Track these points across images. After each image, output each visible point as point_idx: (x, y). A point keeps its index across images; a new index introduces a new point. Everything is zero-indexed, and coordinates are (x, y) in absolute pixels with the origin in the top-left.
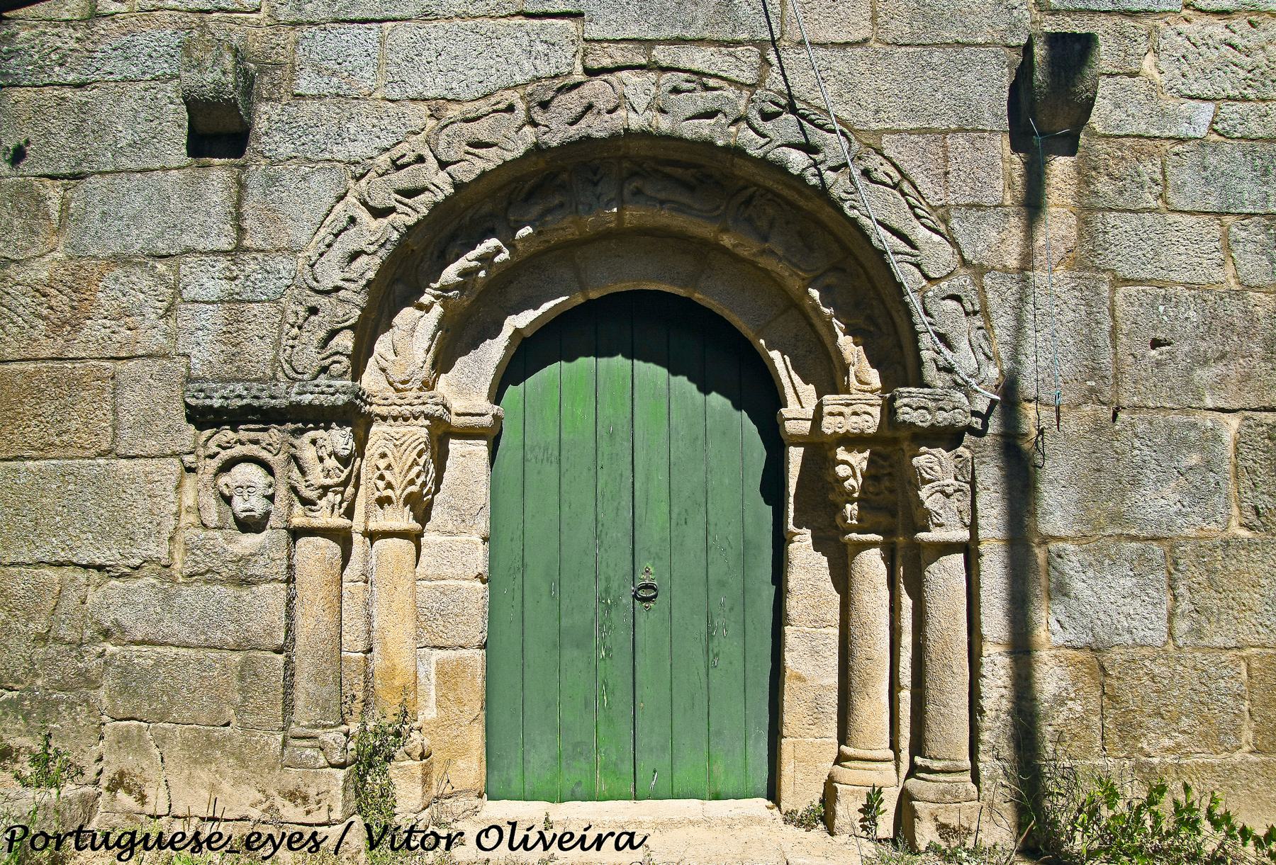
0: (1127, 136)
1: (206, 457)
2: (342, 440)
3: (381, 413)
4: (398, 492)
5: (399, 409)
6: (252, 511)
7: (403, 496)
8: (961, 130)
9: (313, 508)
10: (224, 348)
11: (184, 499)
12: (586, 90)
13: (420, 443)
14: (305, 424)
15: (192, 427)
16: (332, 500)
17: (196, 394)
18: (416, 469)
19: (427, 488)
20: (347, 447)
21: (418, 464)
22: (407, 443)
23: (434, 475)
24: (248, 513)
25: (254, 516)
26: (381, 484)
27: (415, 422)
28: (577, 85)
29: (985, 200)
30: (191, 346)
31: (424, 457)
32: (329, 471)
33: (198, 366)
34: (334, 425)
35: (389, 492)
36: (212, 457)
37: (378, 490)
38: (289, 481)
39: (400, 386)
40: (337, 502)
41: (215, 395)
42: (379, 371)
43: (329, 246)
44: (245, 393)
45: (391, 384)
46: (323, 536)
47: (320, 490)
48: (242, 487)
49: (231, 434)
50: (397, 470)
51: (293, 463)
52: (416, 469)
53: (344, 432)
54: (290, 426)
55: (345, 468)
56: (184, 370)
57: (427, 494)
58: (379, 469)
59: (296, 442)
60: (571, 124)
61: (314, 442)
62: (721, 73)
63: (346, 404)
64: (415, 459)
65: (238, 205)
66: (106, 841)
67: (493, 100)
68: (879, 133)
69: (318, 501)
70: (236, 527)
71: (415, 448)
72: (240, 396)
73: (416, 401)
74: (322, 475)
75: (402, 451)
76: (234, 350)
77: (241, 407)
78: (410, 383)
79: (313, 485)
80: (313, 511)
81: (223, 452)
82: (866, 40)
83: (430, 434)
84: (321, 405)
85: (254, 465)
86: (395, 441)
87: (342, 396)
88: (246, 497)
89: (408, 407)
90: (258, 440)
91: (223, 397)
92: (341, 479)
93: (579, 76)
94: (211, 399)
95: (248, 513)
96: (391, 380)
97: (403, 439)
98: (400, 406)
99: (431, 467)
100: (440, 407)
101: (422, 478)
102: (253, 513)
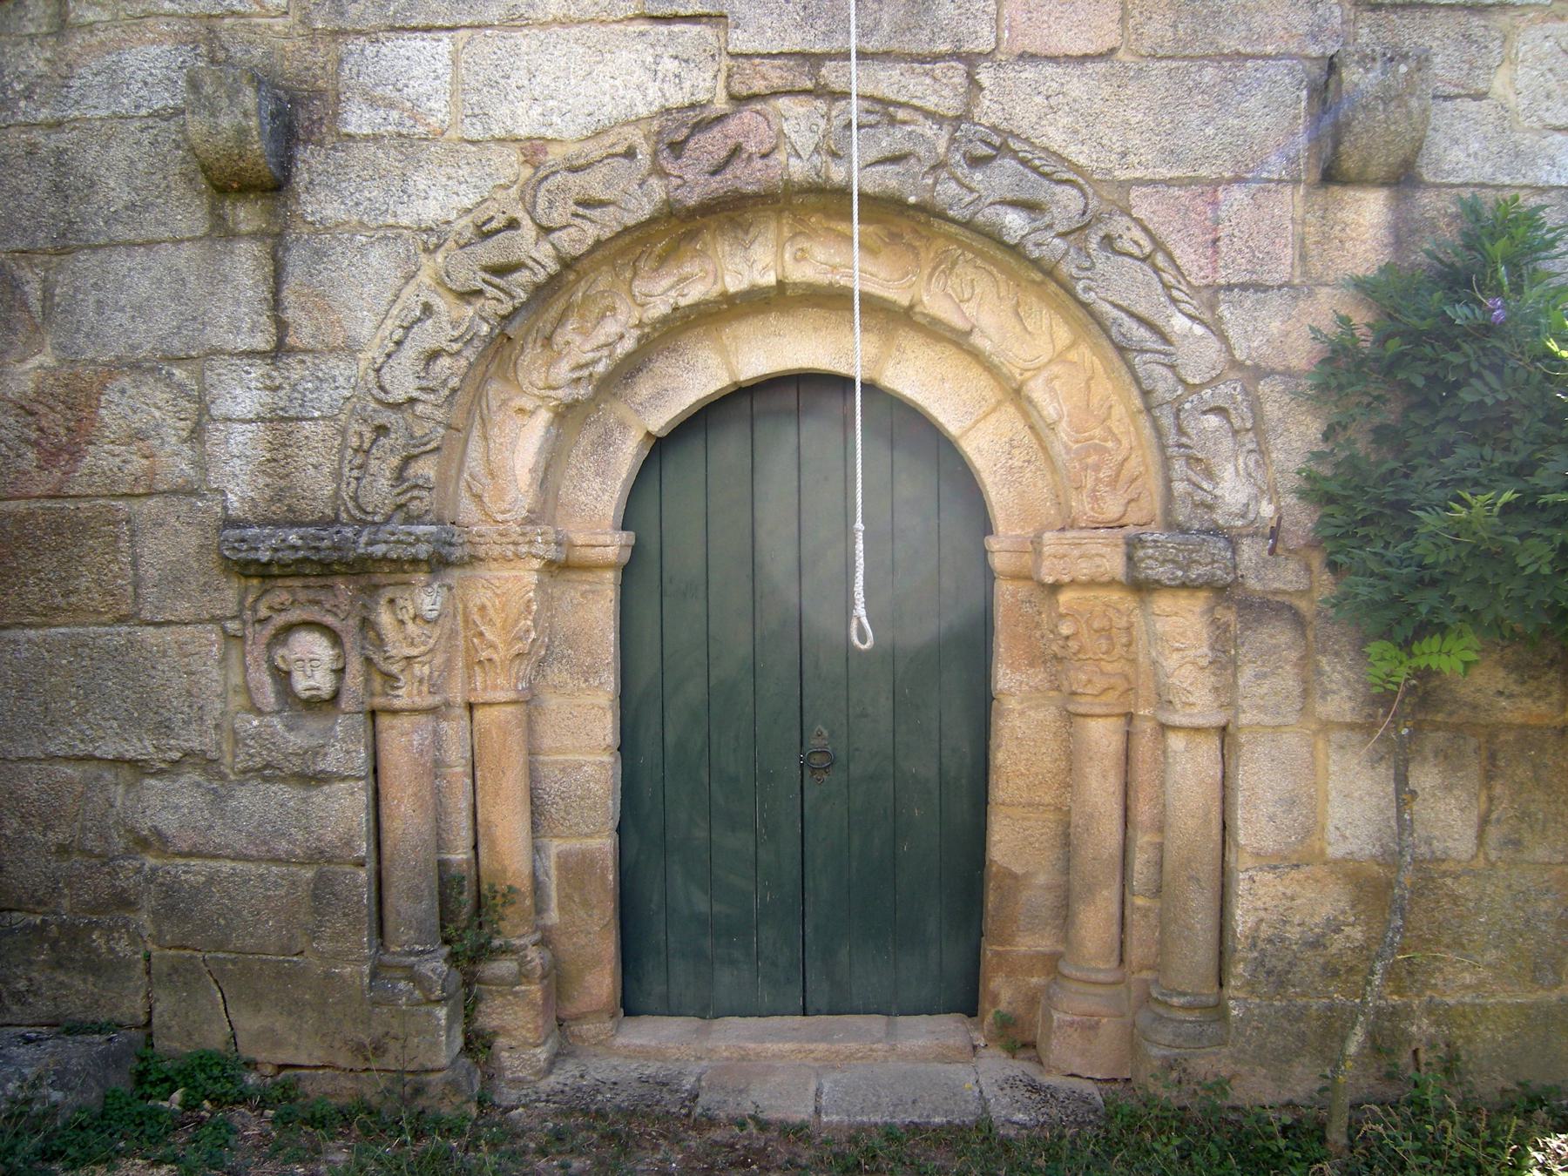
0: (1466, 185)
6: (318, 689)
8: (1238, 180)
10: (269, 480)
12: (732, 126)
28: (721, 119)
29: (1266, 276)
43: (399, 343)
60: (714, 173)
62: (915, 102)
65: (276, 292)
67: (612, 139)
68: (1126, 185)
82: (1112, 51)
89: (510, 547)
93: (721, 104)
95: (314, 692)
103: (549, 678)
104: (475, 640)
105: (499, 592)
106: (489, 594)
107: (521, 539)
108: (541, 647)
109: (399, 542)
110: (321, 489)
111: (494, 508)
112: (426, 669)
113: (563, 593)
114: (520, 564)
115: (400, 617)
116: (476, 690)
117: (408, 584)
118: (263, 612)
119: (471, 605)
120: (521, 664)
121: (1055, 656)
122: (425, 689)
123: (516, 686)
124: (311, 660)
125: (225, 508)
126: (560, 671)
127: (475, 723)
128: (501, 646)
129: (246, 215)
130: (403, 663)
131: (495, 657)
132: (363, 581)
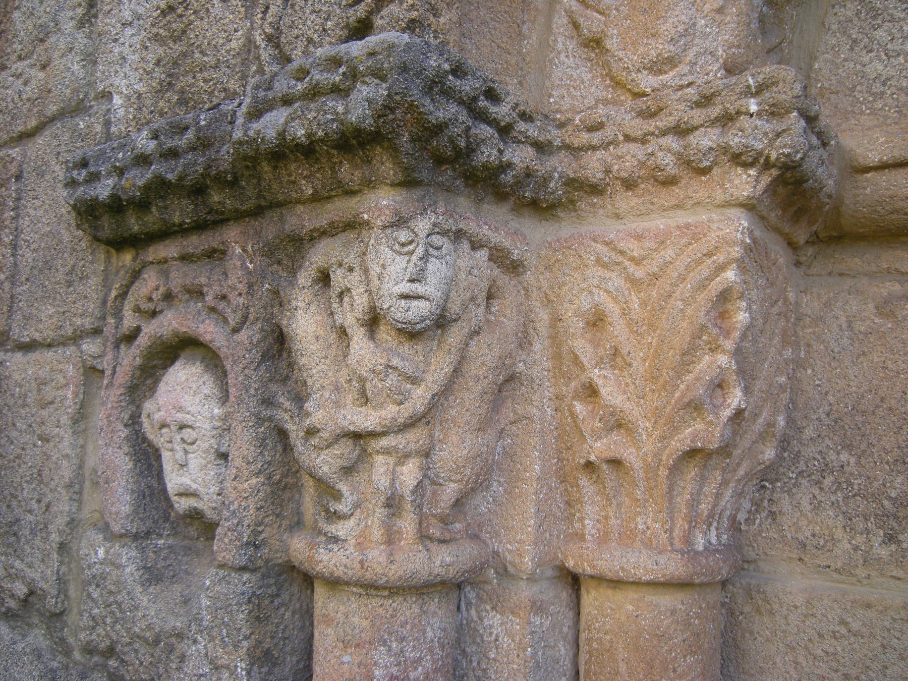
6: (194, 494)
20: (419, 288)
42: (583, 52)
71: (702, 286)
76: (179, 48)
86: (632, 268)
89: (671, 141)
103: (786, 521)
104: (579, 407)
105: (639, 273)
106: (616, 281)
107: (697, 116)
108: (762, 437)
111: (631, 58)
112: (409, 474)
113: (827, 305)
114: (696, 189)
115: (339, 320)
116: (582, 537)
117: (353, 225)
118: (129, 320)
119: (568, 312)
120: (702, 479)
121: (69, 523)
122: (407, 524)
123: (688, 540)
124: (182, 427)
126: (817, 507)
127: (583, 618)
128: (644, 425)
130: (345, 449)
131: (630, 455)
132: (269, 228)
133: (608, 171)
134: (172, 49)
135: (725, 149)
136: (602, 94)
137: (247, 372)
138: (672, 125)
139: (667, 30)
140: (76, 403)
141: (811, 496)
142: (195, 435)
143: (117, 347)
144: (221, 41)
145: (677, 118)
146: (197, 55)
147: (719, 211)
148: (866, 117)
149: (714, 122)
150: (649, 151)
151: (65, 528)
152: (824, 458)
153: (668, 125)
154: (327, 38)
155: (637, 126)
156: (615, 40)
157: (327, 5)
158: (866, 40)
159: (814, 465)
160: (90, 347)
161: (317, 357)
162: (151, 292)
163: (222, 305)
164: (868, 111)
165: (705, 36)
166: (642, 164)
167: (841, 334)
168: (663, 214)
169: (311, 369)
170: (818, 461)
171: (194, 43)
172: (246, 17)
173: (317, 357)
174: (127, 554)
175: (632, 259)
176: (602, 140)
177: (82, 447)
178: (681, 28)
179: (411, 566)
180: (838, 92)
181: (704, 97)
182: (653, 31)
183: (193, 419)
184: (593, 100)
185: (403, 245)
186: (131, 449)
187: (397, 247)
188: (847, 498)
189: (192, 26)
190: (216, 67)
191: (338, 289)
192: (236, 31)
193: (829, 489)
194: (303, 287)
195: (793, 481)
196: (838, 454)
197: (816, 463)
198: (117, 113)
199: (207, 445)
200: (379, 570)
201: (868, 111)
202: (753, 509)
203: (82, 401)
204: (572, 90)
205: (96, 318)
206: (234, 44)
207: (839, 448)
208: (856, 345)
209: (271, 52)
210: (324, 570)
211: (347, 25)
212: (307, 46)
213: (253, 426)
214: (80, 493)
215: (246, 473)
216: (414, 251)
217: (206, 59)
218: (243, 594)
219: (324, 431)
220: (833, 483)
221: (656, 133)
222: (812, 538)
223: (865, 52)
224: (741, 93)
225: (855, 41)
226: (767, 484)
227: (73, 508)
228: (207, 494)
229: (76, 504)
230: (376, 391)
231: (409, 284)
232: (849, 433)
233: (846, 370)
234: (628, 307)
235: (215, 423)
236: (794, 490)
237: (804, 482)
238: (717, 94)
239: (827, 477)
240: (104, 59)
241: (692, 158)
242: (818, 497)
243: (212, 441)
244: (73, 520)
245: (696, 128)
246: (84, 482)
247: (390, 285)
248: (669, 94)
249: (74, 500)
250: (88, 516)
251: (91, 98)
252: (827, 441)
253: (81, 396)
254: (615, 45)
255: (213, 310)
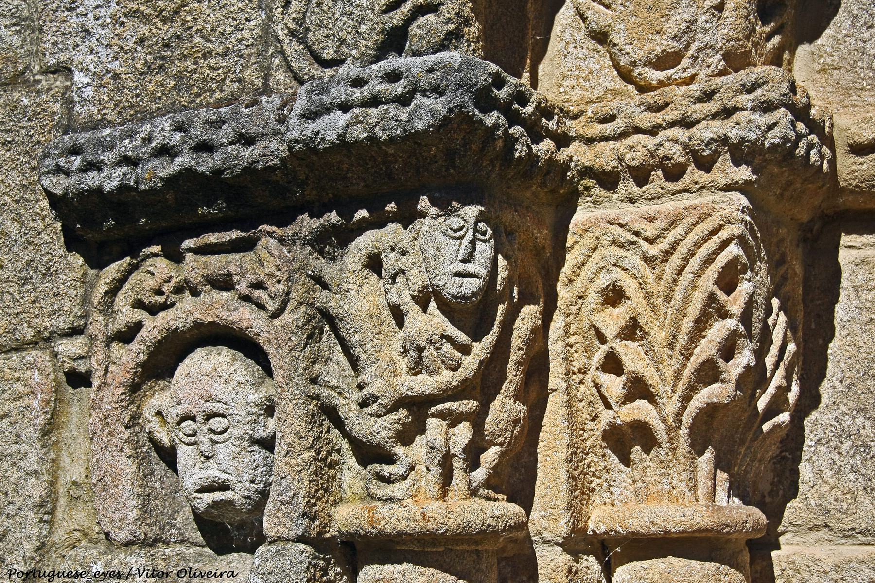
1: (110, 340)
2: (455, 249)
3: (598, 164)
4: (670, 407)
5: (650, 142)
6: (224, 487)
7: (687, 419)
9: (386, 470)
10: (144, 30)
11: (65, 460)
13: (725, 244)
14: (346, 213)
15: (77, 260)
16: (440, 442)
17: (62, 161)
18: (719, 330)
19: (771, 390)
20: (470, 267)
21: (724, 314)
22: (682, 250)
23: (791, 347)
24: (218, 496)
25: (231, 503)
26: (614, 385)
27: (703, 178)
30: (70, 42)
31: (745, 288)
32: (420, 350)
33: (89, 92)
34: (424, 203)
35: (640, 409)
36: (127, 335)
37: (608, 406)
38: (315, 390)
39: (654, 75)
40: (457, 449)
41: (108, 156)
42: (591, 44)
44: (177, 137)
45: (626, 75)
46: (421, 560)
47: (402, 414)
48: (193, 419)
49: (161, 266)
50: (659, 335)
51: (328, 339)
52: (719, 330)
53: (455, 222)
54: (307, 224)
55: (477, 338)
56: (57, 107)
57: (773, 410)
58: (603, 339)
59: (328, 271)
61: (374, 263)
63: (444, 124)
64: (712, 297)
66: (44, 574)
69: (399, 450)
70: (198, 537)
71: (709, 261)
72: (166, 151)
73: (701, 109)
74: (403, 364)
75: (669, 275)
76: (167, 31)
77: (171, 181)
78: (685, 62)
79: (375, 398)
80: (388, 480)
81: (149, 322)
83: (757, 210)
84: (373, 139)
85: (224, 350)
86: (645, 246)
87: (429, 102)
88: (205, 447)
89: (676, 132)
90: (229, 275)
91: (125, 160)
92: (460, 374)
94: (100, 170)
95: (218, 496)
96: (623, 61)
97: (671, 236)
98: (653, 131)
99: (779, 323)
100: (782, 115)
101: (744, 358)
102: (228, 495)
109: (374, 101)
110: (238, 29)
121: (38, 549)
125: (69, 103)
129: (509, 229)
133: (621, 160)
134: (160, 29)
135: (724, 140)
136: (610, 85)
137: (294, 353)
138: (677, 118)
139: (670, 27)
140: (46, 412)
141: (830, 462)
142: (227, 424)
143: (108, 346)
144: (229, 29)
145: (682, 112)
146: (197, 40)
147: (722, 193)
148: (867, 93)
149: (715, 116)
150: (658, 142)
151: (34, 555)
152: (840, 424)
153: (674, 118)
154: (362, 41)
155: (648, 119)
156: (622, 35)
157: (359, 9)
158: (866, 16)
159: (832, 431)
160: (69, 347)
161: (372, 333)
162: (161, 285)
163: (257, 293)
164: (869, 87)
165: (705, 31)
166: (652, 154)
167: (849, 303)
168: (672, 197)
169: (365, 344)
170: (835, 427)
171: (191, 27)
172: (260, 7)
173: (372, 333)
174: (136, 561)
175: (646, 239)
176: (615, 131)
177: (53, 461)
178: (683, 26)
179: (468, 516)
180: (839, 68)
181: (705, 93)
182: (658, 28)
183: (226, 407)
184: (602, 90)
185: (455, 231)
186: (133, 452)
187: (450, 232)
188: (866, 460)
189: (186, 8)
190: (224, 55)
191: (391, 271)
192: (248, 20)
193: (848, 453)
194: (354, 271)
195: (813, 449)
196: (854, 418)
197: (833, 429)
198: (82, 92)
199: (241, 432)
200: (440, 519)
201: (869, 87)
202: (776, 480)
203: (54, 409)
204: (581, 80)
205: (75, 316)
206: (246, 34)
207: (854, 412)
208: (864, 313)
209: (296, 48)
210: (387, 526)
211: (383, 31)
212: (338, 47)
213: (304, 403)
214: (52, 512)
215: (298, 448)
216: (464, 235)
217: (209, 45)
218: (302, 562)
219: (383, 398)
220: (852, 447)
221: (664, 125)
222: (835, 503)
223: (865, 28)
224: (736, 91)
225: (855, 17)
226: (787, 454)
227: (44, 531)
228: (240, 482)
229: (46, 526)
230: (432, 358)
231: (461, 264)
232: (862, 397)
233: (856, 338)
234: (644, 282)
235: (250, 408)
236: (814, 458)
237: (823, 449)
238: (717, 91)
239: (844, 442)
240: (55, 29)
241: (696, 148)
242: (837, 462)
243: (247, 427)
244: (43, 544)
245: (698, 122)
246: (57, 500)
247: (445, 265)
248: (674, 90)
249: (45, 521)
250: (63, 538)
251: (34, 72)
252: (843, 408)
253: (53, 404)
254: (623, 39)
255: (246, 298)
